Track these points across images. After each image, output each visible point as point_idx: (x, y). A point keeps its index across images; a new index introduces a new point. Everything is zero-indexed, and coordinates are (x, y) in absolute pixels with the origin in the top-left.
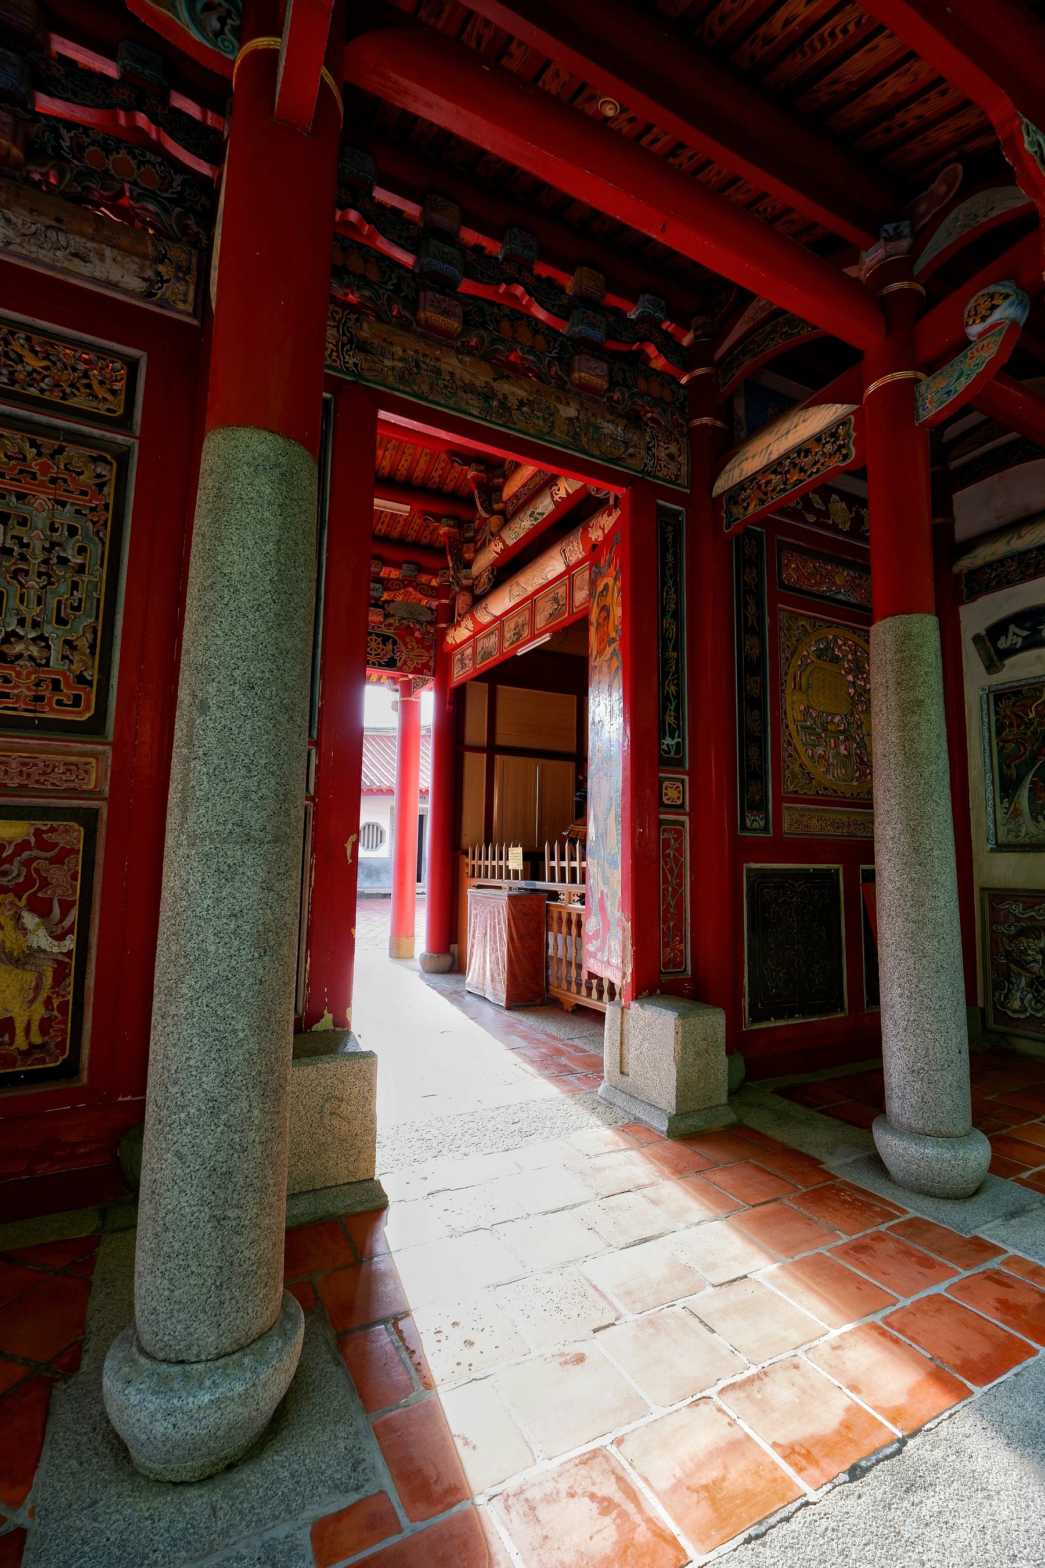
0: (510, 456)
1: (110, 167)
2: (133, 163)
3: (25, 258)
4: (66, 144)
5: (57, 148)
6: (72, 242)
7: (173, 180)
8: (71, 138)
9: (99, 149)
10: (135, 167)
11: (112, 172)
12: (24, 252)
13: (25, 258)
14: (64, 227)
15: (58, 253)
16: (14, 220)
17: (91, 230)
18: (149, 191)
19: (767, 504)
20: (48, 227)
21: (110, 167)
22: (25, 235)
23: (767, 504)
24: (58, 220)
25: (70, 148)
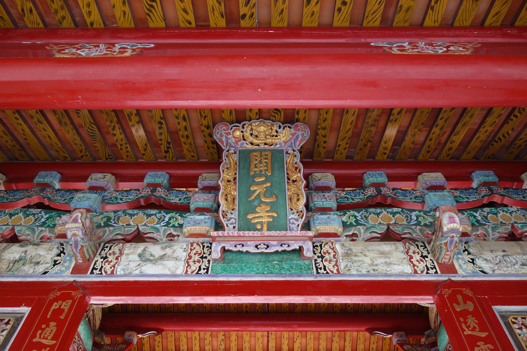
0: (351, 26)
1: (501, 220)
2: (508, 214)
3: (504, 275)
4: (479, 218)
5: (478, 221)
6: (517, 259)
7: (411, 216)
8: (480, 215)
9: (374, 215)
10: (510, 216)
11: (504, 222)
12: (502, 272)
13: (504, 275)
14: (509, 254)
15: (516, 267)
16: (488, 259)
17: (520, 251)
18: (523, 223)
19: (181, 138)
20: (503, 256)
21: (501, 220)
22: (497, 264)
23: (181, 138)
24: (504, 251)
25: (482, 219)
